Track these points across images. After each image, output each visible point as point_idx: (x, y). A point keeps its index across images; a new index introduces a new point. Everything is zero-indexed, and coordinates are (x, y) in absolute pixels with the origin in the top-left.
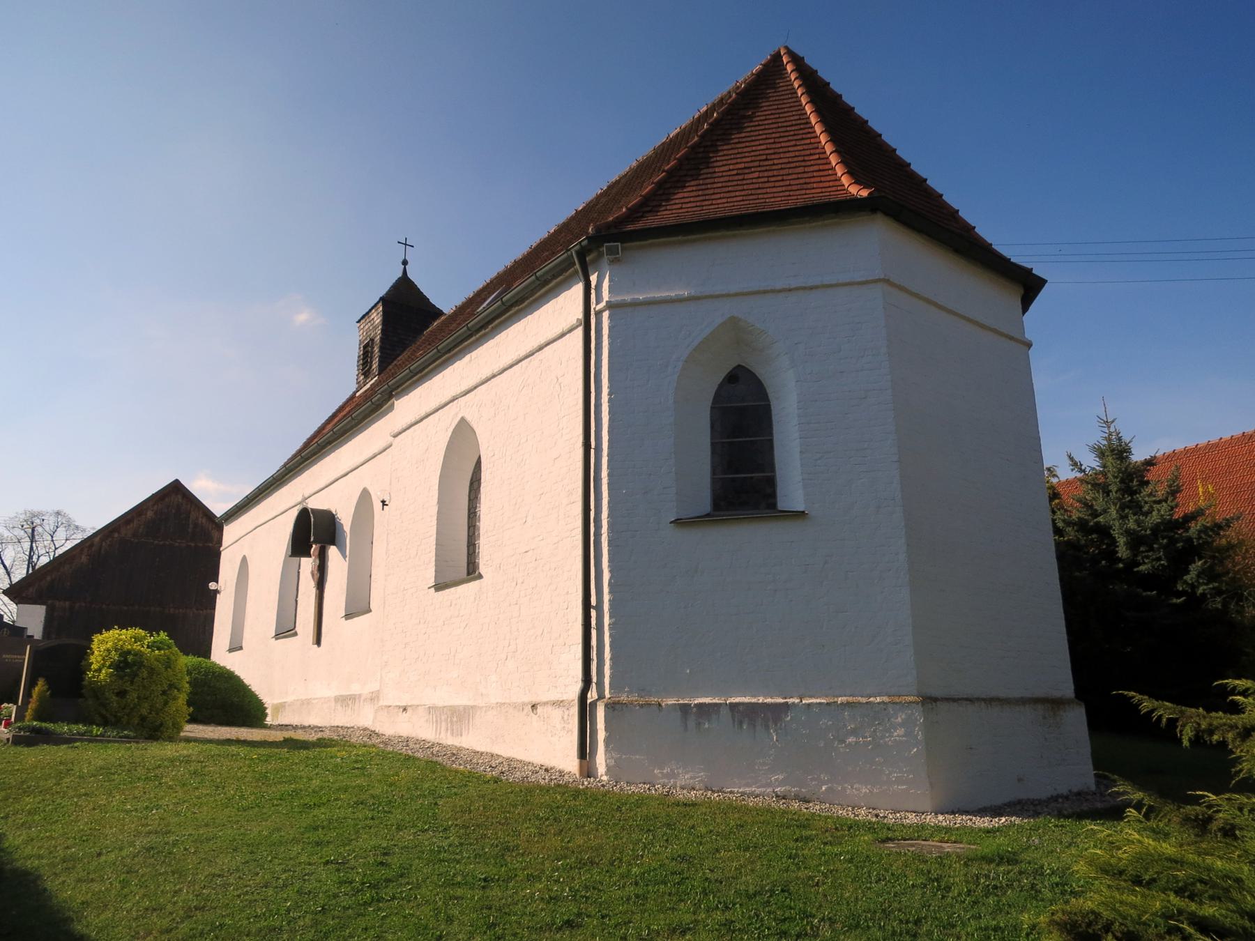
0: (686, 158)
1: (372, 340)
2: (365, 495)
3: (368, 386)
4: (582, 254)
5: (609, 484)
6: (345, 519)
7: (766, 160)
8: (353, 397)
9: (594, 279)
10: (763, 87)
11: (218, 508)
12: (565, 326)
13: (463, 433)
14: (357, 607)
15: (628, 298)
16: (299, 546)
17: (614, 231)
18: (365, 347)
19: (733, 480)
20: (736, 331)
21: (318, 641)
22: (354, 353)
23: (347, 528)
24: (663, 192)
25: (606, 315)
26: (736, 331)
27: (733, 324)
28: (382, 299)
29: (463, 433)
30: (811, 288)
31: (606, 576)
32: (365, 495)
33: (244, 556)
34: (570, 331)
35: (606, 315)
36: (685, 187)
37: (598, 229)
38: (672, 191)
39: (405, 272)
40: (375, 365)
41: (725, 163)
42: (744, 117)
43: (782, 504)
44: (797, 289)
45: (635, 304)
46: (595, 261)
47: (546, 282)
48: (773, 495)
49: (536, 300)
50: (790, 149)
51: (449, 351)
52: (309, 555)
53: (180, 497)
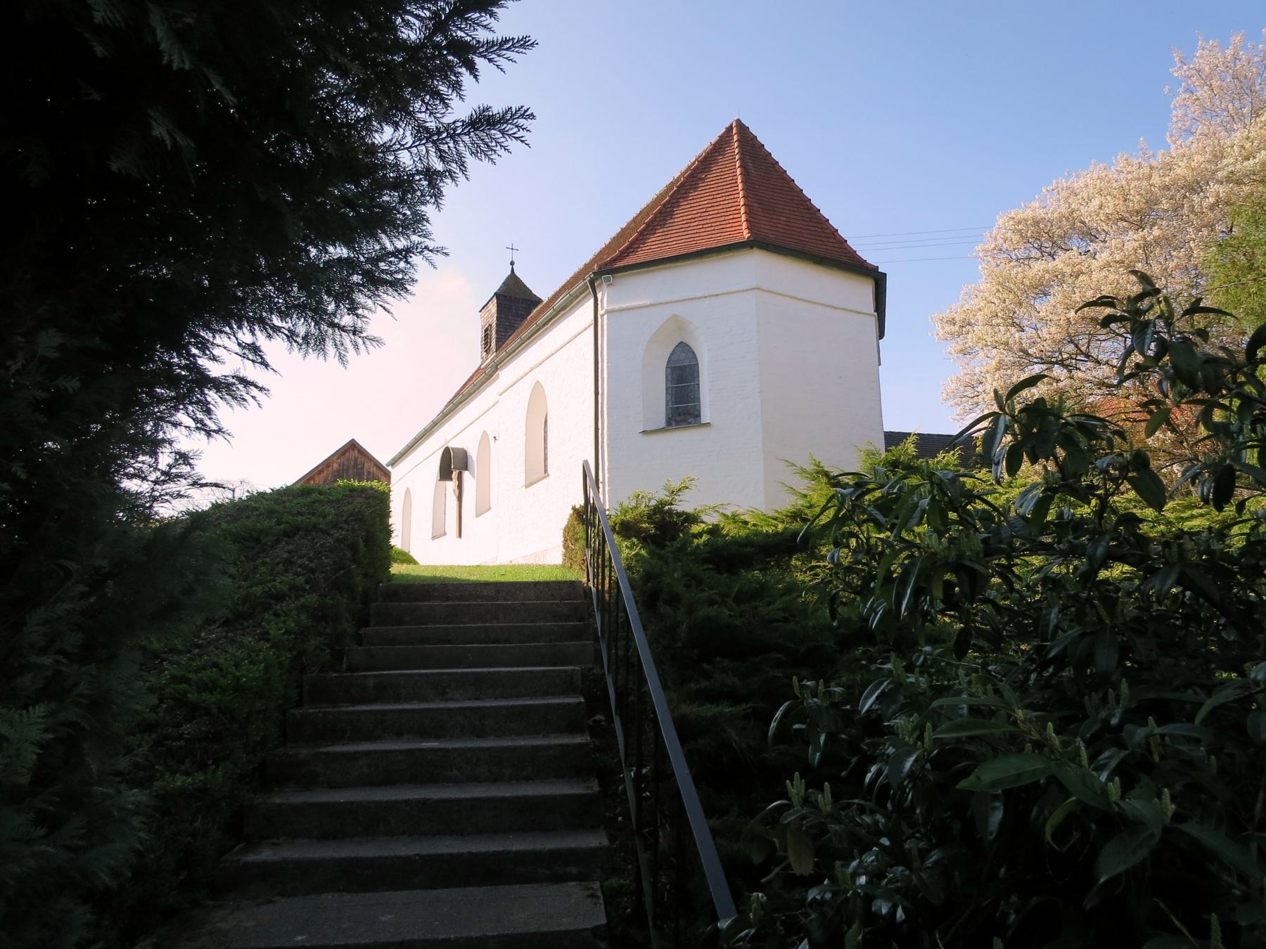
0: (660, 212)
1: (490, 325)
2: (485, 434)
3: (489, 360)
4: (592, 282)
5: (608, 414)
6: (473, 453)
7: (706, 212)
8: (479, 368)
9: (599, 296)
10: (717, 154)
11: (383, 458)
12: (587, 324)
13: (538, 389)
14: (483, 509)
15: (617, 307)
16: (445, 473)
17: (608, 267)
18: (486, 331)
19: (678, 408)
20: (677, 323)
21: (460, 535)
22: (478, 336)
23: (474, 458)
24: (642, 238)
25: (605, 317)
26: (677, 323)
27: (675, 318)
28: (495, 294)
29: (538, 389)
30: (717, 295)
31: (606, 464)
32: (485, 434)
33: (408, 489)
34: (586, 329)
35: (605, 317)
36: (655, 233)
37: (600, 268)
38: (647, 237)
39: (513, 269)
40: (493, 344)
41: (681, 215)
42: (700, 179)
43: (703, 421)
44: (709, 296)
45: (621, 310)
46: (600, 285)
47: (577, 297)
48: (698, 416)
49: (572, 307)
50: (721, 203)
51: (529, 338)
52: (451, 479)
53: (356, 452)
